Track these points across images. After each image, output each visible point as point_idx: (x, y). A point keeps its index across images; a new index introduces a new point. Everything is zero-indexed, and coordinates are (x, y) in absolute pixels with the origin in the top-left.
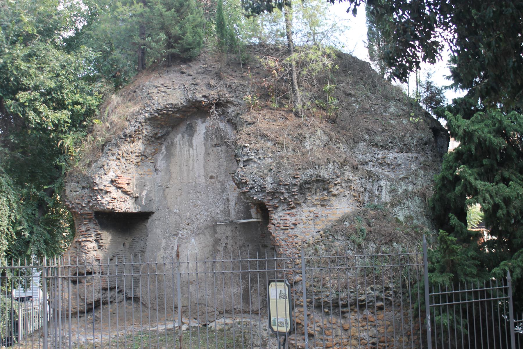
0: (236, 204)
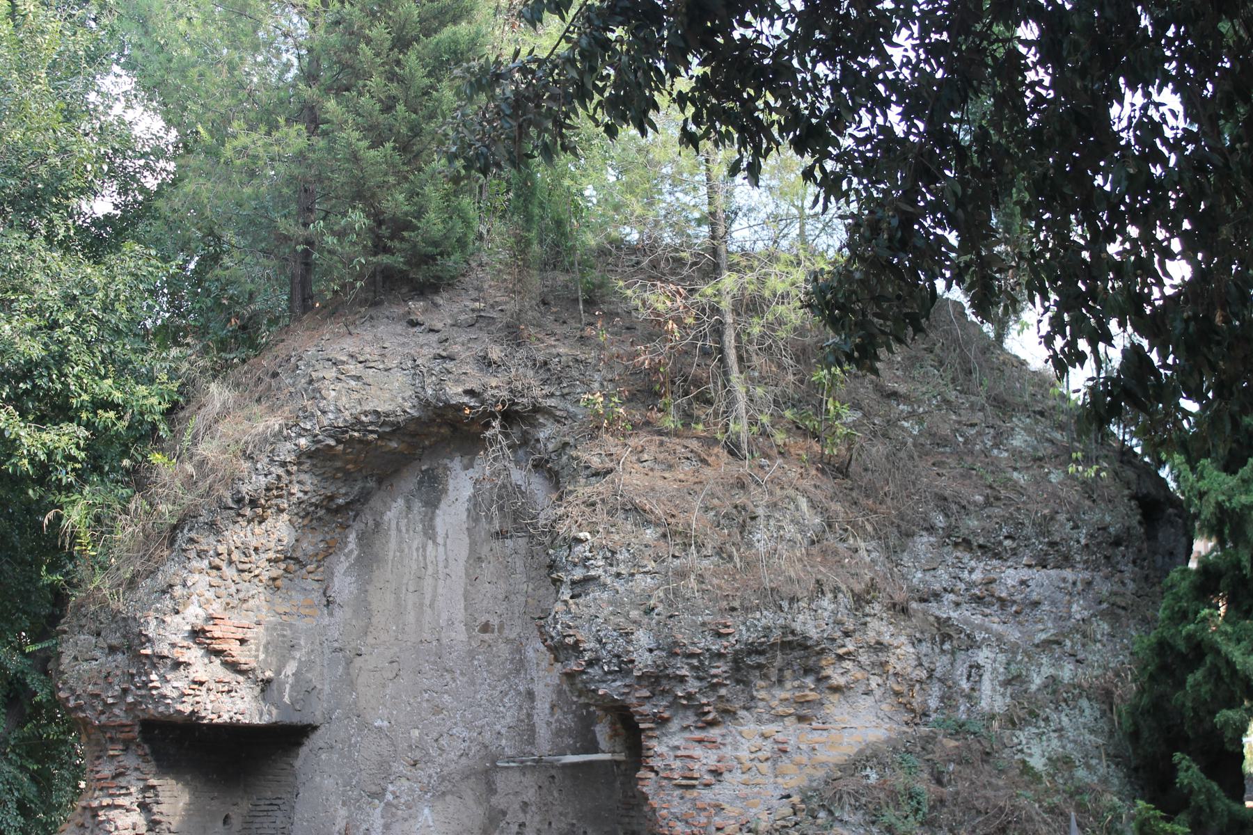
0: (552, 707)
